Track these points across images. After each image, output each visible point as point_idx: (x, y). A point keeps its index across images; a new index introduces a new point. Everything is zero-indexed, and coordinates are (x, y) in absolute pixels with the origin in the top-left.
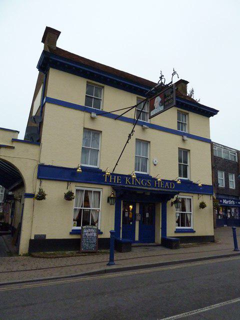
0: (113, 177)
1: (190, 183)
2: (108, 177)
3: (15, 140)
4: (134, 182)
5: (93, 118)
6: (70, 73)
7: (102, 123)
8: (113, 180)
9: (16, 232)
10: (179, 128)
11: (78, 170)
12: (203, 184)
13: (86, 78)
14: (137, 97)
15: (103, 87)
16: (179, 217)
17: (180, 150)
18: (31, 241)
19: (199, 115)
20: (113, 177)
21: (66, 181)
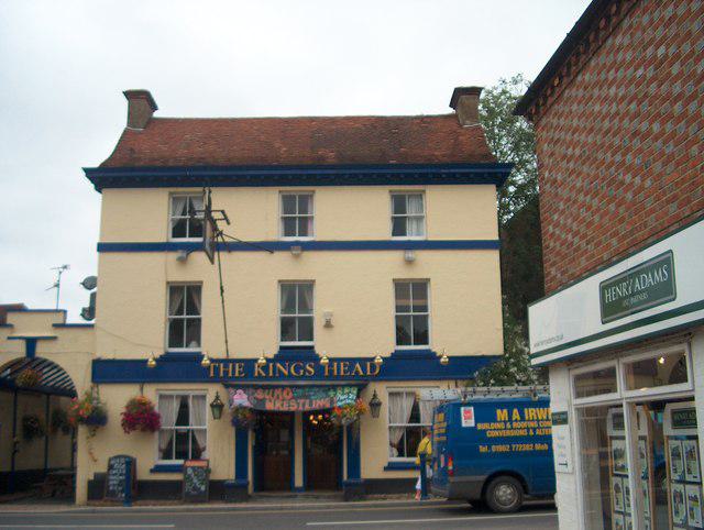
0: (226, 366)
1: (431, 357)
2: (265, 368)
3: (63, 326)
4: (274, 372)
5: (182, 261)
6: (341, 184)
7: (428, 265)
8: (226, 373)
9: (71, 477)
10: (289, 231)
11: (442, 360)
12: (451, 355)
13: (163, 186)
14: (171, 194)
15: (424, 191)
16: (170, 443)
17: (175, 289)
18: (90, 482)
19: (346, 188)
20: (226, 366)
21: (138, 382)
